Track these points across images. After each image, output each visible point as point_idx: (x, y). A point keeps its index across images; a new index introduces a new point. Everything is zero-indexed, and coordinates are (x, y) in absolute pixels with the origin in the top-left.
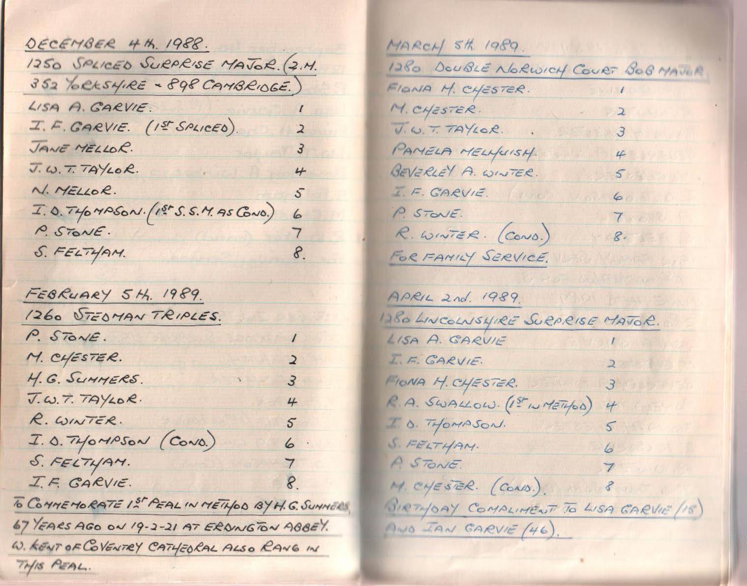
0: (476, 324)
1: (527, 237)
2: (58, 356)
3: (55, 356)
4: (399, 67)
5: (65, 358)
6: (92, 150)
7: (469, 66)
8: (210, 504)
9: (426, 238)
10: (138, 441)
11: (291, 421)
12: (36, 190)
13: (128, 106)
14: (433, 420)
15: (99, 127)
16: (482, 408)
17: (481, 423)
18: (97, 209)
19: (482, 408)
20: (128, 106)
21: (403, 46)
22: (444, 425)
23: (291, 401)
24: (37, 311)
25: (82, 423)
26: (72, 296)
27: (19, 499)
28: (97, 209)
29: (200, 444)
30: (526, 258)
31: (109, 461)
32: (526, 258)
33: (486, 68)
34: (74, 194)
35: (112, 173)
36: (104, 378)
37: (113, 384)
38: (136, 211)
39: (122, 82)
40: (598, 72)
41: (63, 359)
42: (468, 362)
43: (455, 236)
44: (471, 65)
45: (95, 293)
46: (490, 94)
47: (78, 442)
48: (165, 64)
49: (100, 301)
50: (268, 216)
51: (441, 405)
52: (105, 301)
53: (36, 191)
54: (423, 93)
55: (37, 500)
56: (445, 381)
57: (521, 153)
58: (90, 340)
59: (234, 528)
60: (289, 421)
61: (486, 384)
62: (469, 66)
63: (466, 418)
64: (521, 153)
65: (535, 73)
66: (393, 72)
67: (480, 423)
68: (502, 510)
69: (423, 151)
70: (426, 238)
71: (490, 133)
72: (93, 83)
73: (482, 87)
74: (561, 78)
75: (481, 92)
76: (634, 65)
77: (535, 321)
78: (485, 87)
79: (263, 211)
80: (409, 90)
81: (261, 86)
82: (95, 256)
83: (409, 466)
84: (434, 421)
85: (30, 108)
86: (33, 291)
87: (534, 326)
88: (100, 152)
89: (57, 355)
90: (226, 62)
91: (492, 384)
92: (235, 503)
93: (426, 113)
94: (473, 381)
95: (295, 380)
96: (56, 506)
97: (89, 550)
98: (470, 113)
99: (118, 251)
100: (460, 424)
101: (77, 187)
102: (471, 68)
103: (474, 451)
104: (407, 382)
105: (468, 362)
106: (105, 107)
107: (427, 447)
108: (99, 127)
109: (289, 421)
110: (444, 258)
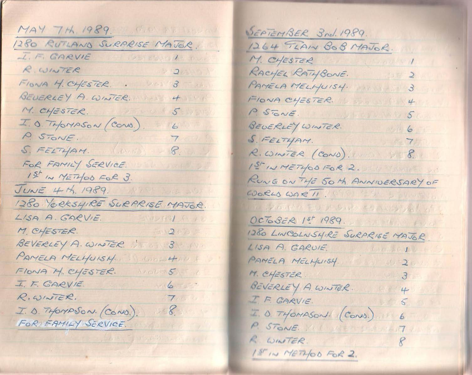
4: (256, 46)
7: (252, 125)
14: (53, 121)
15: (255, 153)
17: (87, 125)
23: (57, 190)
34: (271, 289)
36: (281, 32)
38: (292, 182)
40: (284, 341)
44: (254, 123)
47: (302, 168)
48: (71, 230)
49: (417, 186)
52: (420, 186)
53: (290, 182)
57: (106, 258)
61: (63, 112)
62: (252, 125)
63: (399, 154)
64: (106, 258)
66: (256, 356)
67: (86, 124)
76: (325, 72)
78: (276, 273)
80: (282, 329)
83: (247, 141)
84: (55, 122)
86: (103, 177)
87: (349, 238)
88: (308, 263)
91: (67, 111)
92: (308, 165)
94: (54, 110)
95: (323, 32)
102: (254, 126)
103: (309, 144)
106: (257, 260)
107: (277, 142)
108: (255, 153)
110: (302, 141)
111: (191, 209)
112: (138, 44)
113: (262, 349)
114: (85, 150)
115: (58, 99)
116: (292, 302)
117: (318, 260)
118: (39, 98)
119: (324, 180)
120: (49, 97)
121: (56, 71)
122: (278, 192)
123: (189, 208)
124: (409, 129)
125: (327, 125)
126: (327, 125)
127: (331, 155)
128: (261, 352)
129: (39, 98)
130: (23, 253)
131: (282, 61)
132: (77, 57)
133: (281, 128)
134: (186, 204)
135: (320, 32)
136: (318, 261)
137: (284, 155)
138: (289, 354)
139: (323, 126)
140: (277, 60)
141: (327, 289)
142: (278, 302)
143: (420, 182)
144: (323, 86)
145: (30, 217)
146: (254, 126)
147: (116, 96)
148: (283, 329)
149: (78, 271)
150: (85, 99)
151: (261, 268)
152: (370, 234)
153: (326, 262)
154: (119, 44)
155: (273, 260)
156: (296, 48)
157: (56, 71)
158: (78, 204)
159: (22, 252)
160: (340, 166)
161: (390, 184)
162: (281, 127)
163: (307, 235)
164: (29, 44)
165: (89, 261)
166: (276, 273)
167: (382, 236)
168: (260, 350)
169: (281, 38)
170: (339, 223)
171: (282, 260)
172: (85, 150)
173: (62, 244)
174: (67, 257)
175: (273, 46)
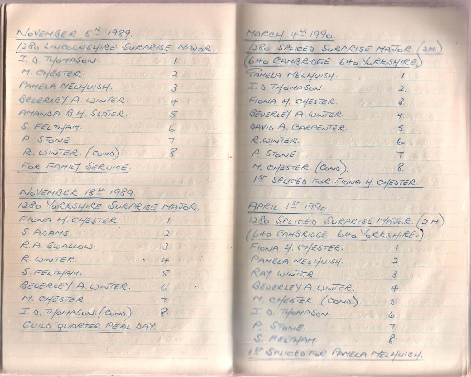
2: (271, 166)
3: (295, 126)
5: (348, 61)
7: (70, 113)
8: (37, 86)
9: (281, 275)
11: (394, 300)
16: (84, 249)
19: (84, 249)
22: (258, 101)
26: (400, 355)
27: (129, 197)
29: (269, 129)
36: (26, 70)
39: (398, 352)
41: (304, 102)
45: (46, 99)
51: (39, 260)
56: (108, 87)
58: (309, 103)
60: (392, 300)
65: (265, 142)
70: (281, 275)
71: (338, 223)
72: (305, 246)
74: (395, 67)
75: (397, 356)
77: (328, 49)
82: (308, 250)
88: (53, 102)
89: (44, 298)
96: (34, 87)
99: (269, 260)
100: (295, 88)
109: (392, 300)
112: (324, 75)
115: (55, 102)
118: (266, 115)
120: (47, 100)
125: (111, 99)
126: (111, 99)
127: (341, 302)
129: (266, 115)
130: (257, 151)
131: (308, 102)
133: (276, 116)
134: (393, 47)
135: (174, 87)
137: (57, 153)
138: (65, 62)
141: (329, 289)
146: (257, 114)
149: (310, 75)
150: (303, 116)
159: (256, 150)
160: (140, 46)
161: (98, 168)
162: (276, 115)
163: (82, 48)
164: (33, 47)
165: (314, 78)
169: (289, 114)
170: (176, 100)
171: (300, 113)
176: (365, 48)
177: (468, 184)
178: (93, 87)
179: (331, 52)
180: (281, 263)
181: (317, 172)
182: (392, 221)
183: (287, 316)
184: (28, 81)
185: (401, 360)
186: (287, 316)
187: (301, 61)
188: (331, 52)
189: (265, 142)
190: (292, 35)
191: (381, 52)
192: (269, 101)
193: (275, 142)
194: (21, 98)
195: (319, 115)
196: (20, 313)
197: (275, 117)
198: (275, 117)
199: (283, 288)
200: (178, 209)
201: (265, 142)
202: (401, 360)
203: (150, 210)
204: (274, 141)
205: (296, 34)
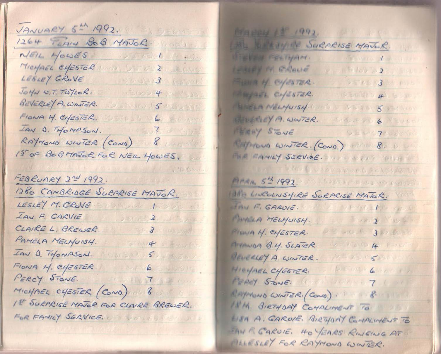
0: (58, 307)
1: (115, 293)
6: (293, 296)
7: (23, 102)
10: (62, 254)
12: (93, 132)
13: (32, 103)
18: (16, 289)
20: (32, 103)
21: (74, 155)
24: (22, 218)
25: (77, 44)
28: (16, 289)
30: (23, 292)
31: (366, 195)
32: (23, 292)
33: (292, 295)
35: (275, 196)
37: (24, 208)
42: (75, 217)
43: (289, 296)
46: (72, 294)
50: (328, 298)
54: (39, 320)
55: (106, 291)
59: (279, 295)
62: (23, 102)
68: (25, 31)
69: (58, 240)
73: (280, 231)
79: (120, 291)
81: (118, 292)
85: (22, 80)
90: (72, 129)
93: (30, 293)
97: (313, 297)
98: (298, 297)
101: (85, 290)
104: (278, 295)
105: (75, 217)
109: (157, 106)
111: (163, 197)
113: (22, 300)
114: (58, 203)
116: (90, 268)
117: (76, 241)
119: (157, 106)
121: (295, 259)
122: (44, 127)
123: (160, 197)
124: (379, 121)
128: (21, 302)
132: (158, 194)
136: (76, 92)
139: (302, 119)
140: (277, 271)
142: (53, 217)
143: (53, 103)
144: (290, 220)
145: (130, 193)
147: (303, 257)
148: (299, 31)
151: (246, 227)
152: (109, 192)
153: (296, 220)
154: (163, 194)
155: (65, 241)
156: (121, 156)
157: (295, 259)
158: (287, 195)
166: (68, 290)
167: (131, 193)
168: (20, 301)
172: (58, 203)
173: (266, 255)
174: (146, 193)
175: (374, 246)
176: (132, 193)
177: (367, 353)
178: (294, 220)
179: (104, 196)
180: (68, 243)
181: (305, 301)
182: (370, 44)
183: (249, 274)
184: (323, 305)
185: (328, 200)
186: (249, 274)
187: (30, 179)
188: (104, 196)
189: (158, 157)
190: (149, 245)
191: (90, 182)
192: (31, 267)
193: (360, 346)
194: (267, 245)
195: (376, 321)
196: (20, 117)
197: (72, 231)
198: (72, 231)
199: (262, 272)
200: (156, 196)
201: (158, 157)
202: (328, 200)
203: (101, 196)
204: (122, 145)
205: (153, 243)
